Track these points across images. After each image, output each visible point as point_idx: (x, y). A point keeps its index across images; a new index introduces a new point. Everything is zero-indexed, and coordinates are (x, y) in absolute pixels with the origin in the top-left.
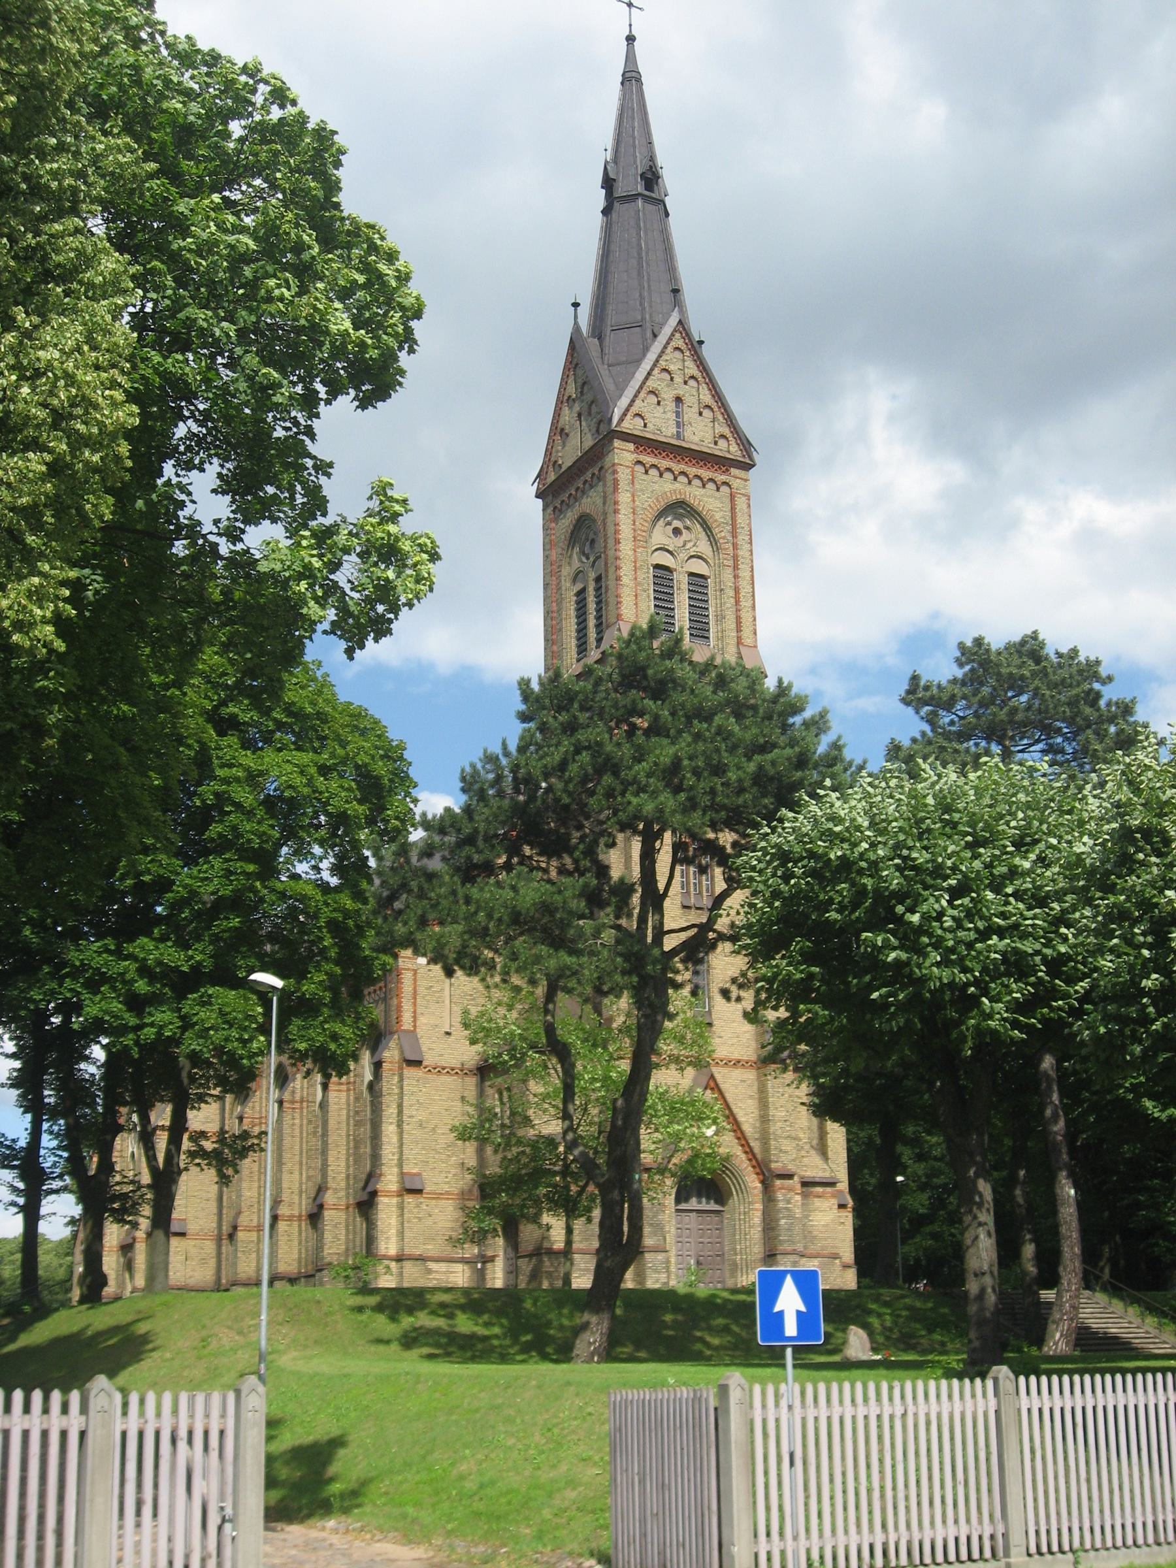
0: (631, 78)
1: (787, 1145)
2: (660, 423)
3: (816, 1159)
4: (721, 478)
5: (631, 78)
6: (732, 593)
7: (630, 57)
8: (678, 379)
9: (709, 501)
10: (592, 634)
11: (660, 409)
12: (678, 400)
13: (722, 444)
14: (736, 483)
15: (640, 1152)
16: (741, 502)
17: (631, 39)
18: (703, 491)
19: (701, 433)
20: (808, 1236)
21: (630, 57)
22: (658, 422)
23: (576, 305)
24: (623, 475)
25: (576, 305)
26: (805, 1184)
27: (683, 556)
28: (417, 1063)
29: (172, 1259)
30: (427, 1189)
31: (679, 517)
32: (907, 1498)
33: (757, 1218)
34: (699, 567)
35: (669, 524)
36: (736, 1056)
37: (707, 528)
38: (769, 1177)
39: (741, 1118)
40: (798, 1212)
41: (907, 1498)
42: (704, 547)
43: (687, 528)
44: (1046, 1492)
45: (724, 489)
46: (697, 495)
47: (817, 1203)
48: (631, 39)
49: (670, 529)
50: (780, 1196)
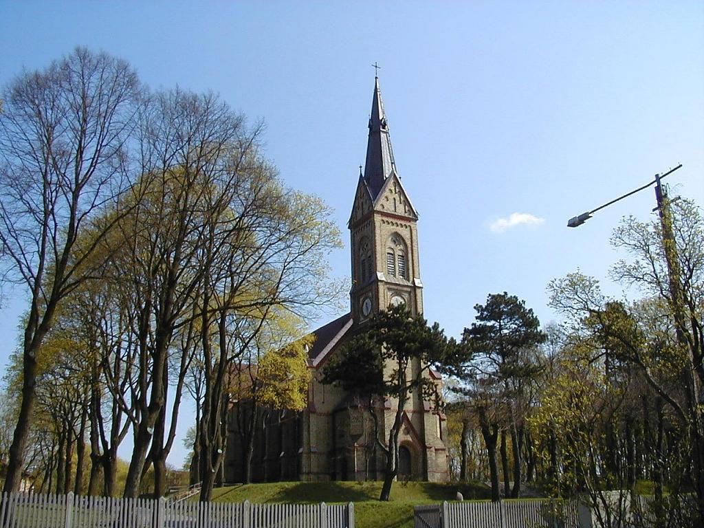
1: (431, 438)
2: (389, 208)
3: (440, 441)
4: (408, 224)
9: (405, 233)
10: (367, 275)
12: (394, 199)
14: (412, 226)
16: (414, 232)
19: (401, 210)
20: (437, 466)
23: (361, 167)
24: (377, 224)
25: (361, 167)
26: (436, 450)
28: (314, 413)
29: (377, 256)
30: (392, 408)
32: (235, 515)
33: (421, 461)
40: (434, 458)
41: (235, 515)
44: (258, 519)
47: (440, 455)
50: (428, 453)
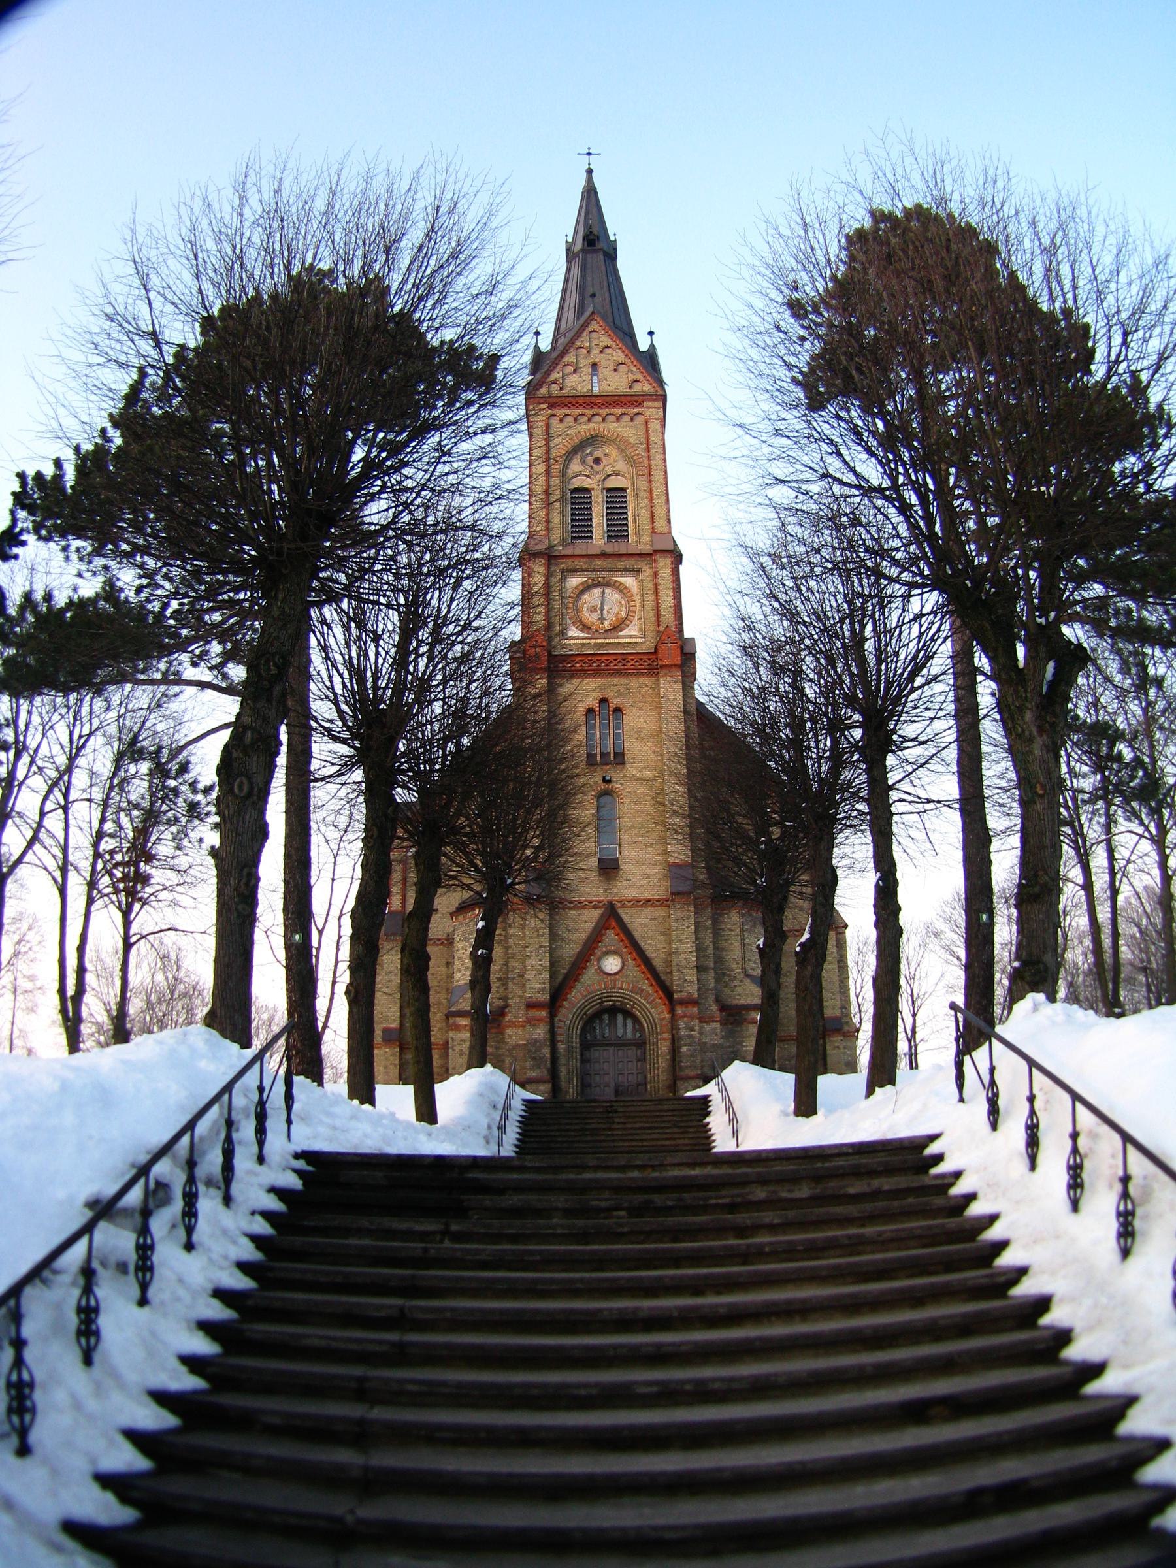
5: (590, 195)
6: (646, 495)
8: (595, 351)
17: (590, 172)
34: (613, 483)
36: (646, 896)
39: (651, 952)
48: (590, 172)
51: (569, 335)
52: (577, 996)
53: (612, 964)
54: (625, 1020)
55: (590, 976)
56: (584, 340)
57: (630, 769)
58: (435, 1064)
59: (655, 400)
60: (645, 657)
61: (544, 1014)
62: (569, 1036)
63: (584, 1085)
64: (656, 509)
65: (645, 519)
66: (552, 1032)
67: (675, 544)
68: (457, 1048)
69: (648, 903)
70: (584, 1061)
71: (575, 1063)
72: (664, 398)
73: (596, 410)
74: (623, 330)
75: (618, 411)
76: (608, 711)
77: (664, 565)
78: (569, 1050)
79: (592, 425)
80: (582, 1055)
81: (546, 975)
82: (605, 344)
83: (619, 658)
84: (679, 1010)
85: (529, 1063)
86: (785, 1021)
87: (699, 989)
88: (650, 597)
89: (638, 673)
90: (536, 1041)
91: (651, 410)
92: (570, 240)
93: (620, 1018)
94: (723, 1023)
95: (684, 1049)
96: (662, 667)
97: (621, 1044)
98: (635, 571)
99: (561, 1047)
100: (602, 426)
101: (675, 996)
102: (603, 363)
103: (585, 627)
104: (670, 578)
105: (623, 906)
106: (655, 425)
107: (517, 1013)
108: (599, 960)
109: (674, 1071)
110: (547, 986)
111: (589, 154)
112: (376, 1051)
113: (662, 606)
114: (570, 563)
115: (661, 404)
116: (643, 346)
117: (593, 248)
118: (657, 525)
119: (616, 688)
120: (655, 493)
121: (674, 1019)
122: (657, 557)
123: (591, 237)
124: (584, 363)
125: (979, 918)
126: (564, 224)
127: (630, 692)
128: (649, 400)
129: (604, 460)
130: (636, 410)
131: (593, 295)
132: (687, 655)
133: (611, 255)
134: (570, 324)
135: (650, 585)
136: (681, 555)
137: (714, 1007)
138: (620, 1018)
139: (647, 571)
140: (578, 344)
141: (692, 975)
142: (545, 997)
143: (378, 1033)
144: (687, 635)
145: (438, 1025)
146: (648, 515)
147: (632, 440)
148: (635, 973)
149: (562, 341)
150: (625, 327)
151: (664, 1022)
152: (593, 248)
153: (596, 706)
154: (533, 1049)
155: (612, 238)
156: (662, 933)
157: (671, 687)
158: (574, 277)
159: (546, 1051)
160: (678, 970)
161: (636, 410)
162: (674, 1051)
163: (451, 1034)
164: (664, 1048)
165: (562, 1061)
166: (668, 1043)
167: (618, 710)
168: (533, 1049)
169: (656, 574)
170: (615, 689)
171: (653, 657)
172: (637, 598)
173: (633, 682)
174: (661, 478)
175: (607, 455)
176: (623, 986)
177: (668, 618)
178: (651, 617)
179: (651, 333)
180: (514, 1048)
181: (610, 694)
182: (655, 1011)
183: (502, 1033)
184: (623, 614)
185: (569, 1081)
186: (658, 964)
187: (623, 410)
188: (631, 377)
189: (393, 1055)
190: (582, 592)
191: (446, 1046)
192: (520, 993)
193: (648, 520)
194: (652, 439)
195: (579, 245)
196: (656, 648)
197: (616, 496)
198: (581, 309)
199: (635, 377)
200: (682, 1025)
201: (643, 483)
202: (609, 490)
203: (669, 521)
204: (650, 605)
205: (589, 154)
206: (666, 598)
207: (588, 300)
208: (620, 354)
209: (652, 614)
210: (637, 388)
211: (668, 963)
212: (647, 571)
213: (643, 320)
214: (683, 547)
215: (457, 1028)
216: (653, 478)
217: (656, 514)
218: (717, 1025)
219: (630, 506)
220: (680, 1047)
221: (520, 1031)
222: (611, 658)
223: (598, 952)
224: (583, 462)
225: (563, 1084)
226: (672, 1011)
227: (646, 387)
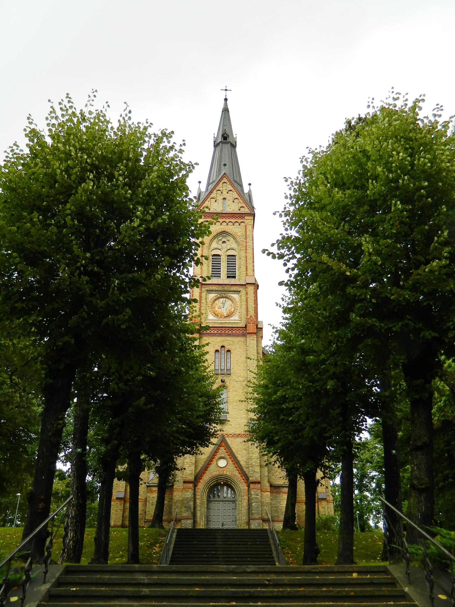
0: (226, 111)
4: (240, 221)
5: (226, 111)
6: (244, 259)
7: (226, 104)
8: (225, 192)
11: (216, 203)
13: (242, 209)
15: (250, 530)
17: (226, 100)
18: (233, 227)
21: (226, 104)
22: (215, 208)
23: (200, 182)
27: (225, 250)
31: (224, 237)
34: (231, 253)
35: (221, 240)
36: (238, 432)
37: (235, 238)
38: (249, 483)
39: (239, 458)
42: (234, 245)
43: (228, 240)
45: (242, 224)
46: (230, 228)
48: (226, 100)
49: (221, 242)
51: (214, 184)
52: (206, 477)
53: (222, 463)
54: (228, 490)
55: (212, 467)
56: (220, 187)
57: (233, 377)
58: (140, 509)
59: (250, 216)
60: (241, 329)
61: (191, 485)
62: (202, 498)
63: (208, 521)
64: (248, 265)
65: (243, 268)
66: (195, 494)
67: (256, 280)
68: (151, 502)
69: (239, 435)
70: (208, 508)
71: (204, 510)
72: (254, 215)
73: (224, 220)
74: (237, 183)
75: (233, 220)
76: (224, 351)
77: (251, 289)
78: (202, 503)
79: (222, 226)
80: (207, 505)
81: (193, 467)
82: (229, 189)
83: (230, 329)
84: (252, 486)
85: (183, 509)
86: (300, 493)
87: (261, 476)
88: (244, 303)
89: (238, 335)
90: (187, 498)
91: (248, 220)
92: (216, 136)
93: (225, 488)
94: (271, 492)
95: (254, 504)
96: (248, 333)
97: (225, 501)
98: (238, 292)
99: (198, 501)
100: (227, 227)
101: (250, 479)
102: (228, 198)
103: (216, 315)
104: (253, 295)
105: (228, 436)
106: (249, 228)
107: (178, 485)
108: (217, 461)
109: (249, 514)
110: (193, 472)
111: (226, 90)
112: (112, 503)
113: (249, 307)
114: (211, 288)
115: (252, 218)
116: (246, 190)
117: (225, 141)
118: (248, 272)
119: (228, 341)
120: (248, 258)
121: (249, 490)
122: (247, 286)
123: (225, 135)
124: (220, 198)
125: (391, 452)
126: (213, 129)
127: (234, 343)
128: (247, 216)
129: (227, 242)
130: (242, 220)
131: (225, 165)
132: (259, 330)
133: (234, 146)
134: (214, 179)
135: (244, 298)
136: (258, 286)
137: (268, 485)
138: (225, 488)
139: (243, 292)
140: (218, 188)
141: (257, 469)
142: (192, 478)
143: (114, 497)
144: (259, 319)
145: (143, 490)
146: (244, 267)
147: (239, 234)
148: (232, 467)
149: (211, 187)
150: (238, 181)
151: (245, 491)
152: (225, 141)
153: (219, 349)
154: (186, 502)
155: (235, 137)
156: (245, 449)
157: (252, 341)
158: (217, 156)
159: (192, 503)
160: (252, 467)
161: (242, 220)
162: (249, 505)
163: (148, 494)
164: (245, 503)
165: (198, 508)
166: (246, 501)
167: (229, 351)
168: (186, 502)
169: (247, 293)
170: (228, 342)
171: (244, 329)
172: (238, 303)
173: (236, 339)
174: (251, 251)
175: (228, 240)
176: (227, 472)
177: (251, 312)
178: (244, 312)
179: (250, 184)
180: (177, 502)
181: (225, 344)
182: (242, 486)
183: (172, 494)
184: (233, 310)
185: (201, 518)
186: (243, 463)
187: (236, 220)
188: (240, 205)
189: (121, 505)
190: (215, 300)
191: (146, 500)
192: (181, 475)
193: (245, 270)
194: (248, 233)
195: (220, 139)
196: (246, 325)
197: (231, 258)
198: (219, 171)
199: (242, 205)
200: (253, 493)
201: (243, 254)
202: (228, 256)
203: (254, 271)
204: (244, 307)
205: (226, 90)
206: (250, 304)
207: (223, 167)
208: (236, 194)
209: (245, 310)
210: (243, 211)
211: (247, 463)
212: (243, 292)
213: (246, 177)
214: (259, 282)
215: (152, 492)
216: (248, 251)
217: (248, 267)
218: (269, 493)
219: (237, 263)
220: (251, 503)
221: (180, 493)
222: (227, 329)
223: (217, 457)
224: (217, 243)
225: (198, 520)
226: (249, 486)
227: (246, 210)
